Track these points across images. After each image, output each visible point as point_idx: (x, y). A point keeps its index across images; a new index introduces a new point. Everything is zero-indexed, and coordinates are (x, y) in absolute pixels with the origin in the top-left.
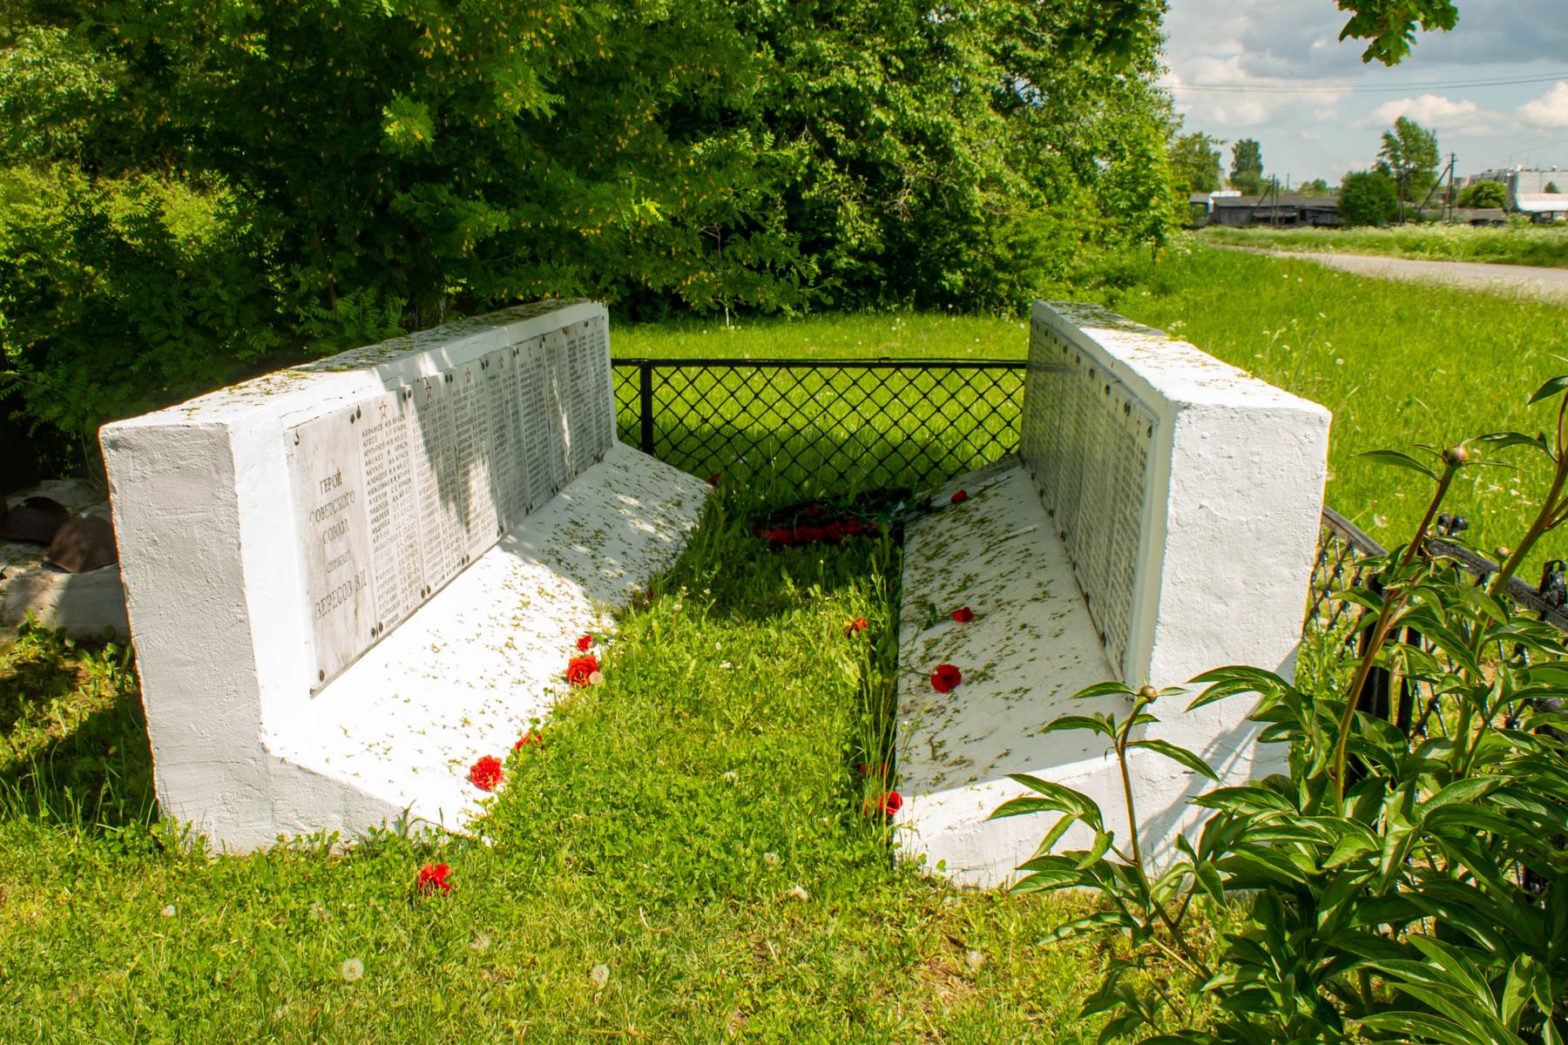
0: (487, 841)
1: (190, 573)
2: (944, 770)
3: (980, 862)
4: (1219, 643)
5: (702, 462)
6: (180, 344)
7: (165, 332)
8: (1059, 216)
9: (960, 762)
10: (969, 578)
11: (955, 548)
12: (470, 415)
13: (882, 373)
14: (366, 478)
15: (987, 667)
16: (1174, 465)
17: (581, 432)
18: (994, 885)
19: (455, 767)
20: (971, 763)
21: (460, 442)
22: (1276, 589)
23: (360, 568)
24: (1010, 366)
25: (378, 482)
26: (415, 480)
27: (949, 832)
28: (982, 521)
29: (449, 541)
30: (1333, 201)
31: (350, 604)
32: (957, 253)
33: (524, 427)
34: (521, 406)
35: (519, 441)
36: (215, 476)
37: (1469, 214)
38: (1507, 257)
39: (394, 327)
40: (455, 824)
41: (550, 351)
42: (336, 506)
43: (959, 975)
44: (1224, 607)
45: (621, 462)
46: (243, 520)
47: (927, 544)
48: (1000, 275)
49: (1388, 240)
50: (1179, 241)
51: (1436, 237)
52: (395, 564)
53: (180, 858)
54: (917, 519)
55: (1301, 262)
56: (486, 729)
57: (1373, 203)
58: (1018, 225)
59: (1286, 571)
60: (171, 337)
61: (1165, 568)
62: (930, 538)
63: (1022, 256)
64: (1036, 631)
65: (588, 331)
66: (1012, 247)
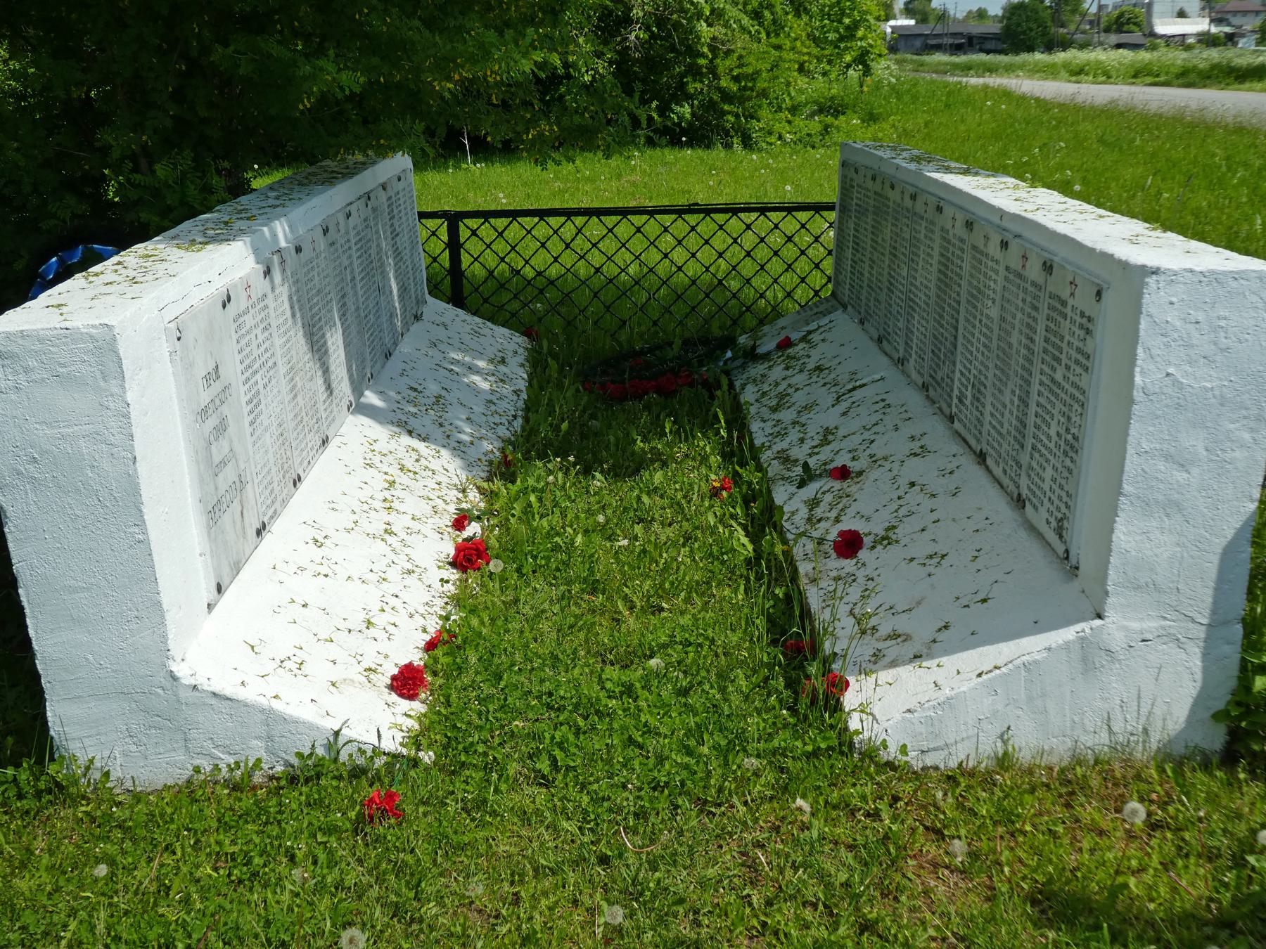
0: (427, 757)
1: (78, 491)
2: (881, 645)
3: (940, 743)
4: (1180, 511)
5: (513, 315)
8: (778, 47)
9: (894, 636)
10: (828, 431)
11: (800, 398)
13: (692, 219)
14: (240, 367)
15: (888, 529)
16: (1142, 333)
18: (953, 763)
20: (908, 638)
21: (313, 316)
22: (1237, 454)
23: (242, 466)
24: (818, 208)
25: (249, 369)
26: (280, 363)
27: (908, 715)
28: (819, 369)
30: (996, 28)
31: (236, 506)
32: (682, 86)
33: (360, 293)
34: (357, 271)
35: (358, 308)
36: (102, 384)
37: (1114, 38)
38: (1162, 79)
40: (392, 743)
41: (374, 210)
42: (217, 402)
43: (947, 867)
44: (1185, 475)
45: (438, 319)
46: (137, 432)
47: (764, 394)
48: (726, 107)
49: (1054, 65)
50: (885, 68)
51: (1099, 62)
52: (270, 455)
53: (84, 797)
54: (744, 367)
55: (995, 90)
56: (391, 629)
57: (1031, 30)
58: (740, 57)
59: (1247, 436)
61: (1130, 439)
62: (766, 388)
63: (745, 88)
64: (928, 489)
65: (402, 184)
66: (736, 79)
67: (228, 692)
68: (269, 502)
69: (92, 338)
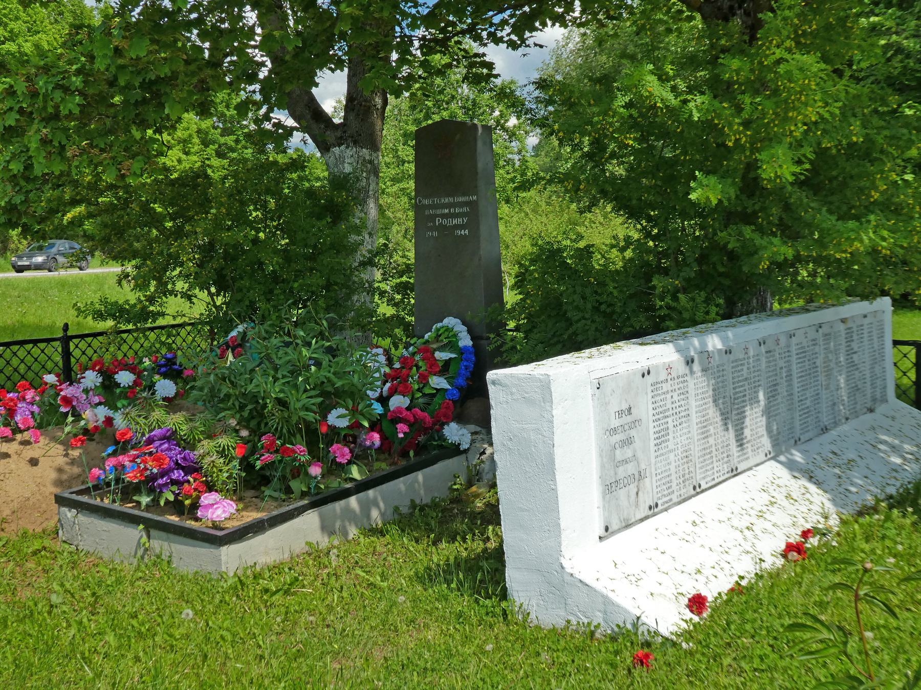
1: (528, 459)
6: (589, 322)
7: (581, 315)
12: (745, 376)
17: (855, 390)
19: (680, 597)
23: (643, 466)
25: (661, 415)
29: (720, 457)
31: (633, 488)
39: (713, 315)
42: (626, 427)
46: (557, 432)
52: (672, 467)
60: (584, 318)
65: (866, 321)
67: (587, 582)
68: (666, 492)
69: (541, 381)
